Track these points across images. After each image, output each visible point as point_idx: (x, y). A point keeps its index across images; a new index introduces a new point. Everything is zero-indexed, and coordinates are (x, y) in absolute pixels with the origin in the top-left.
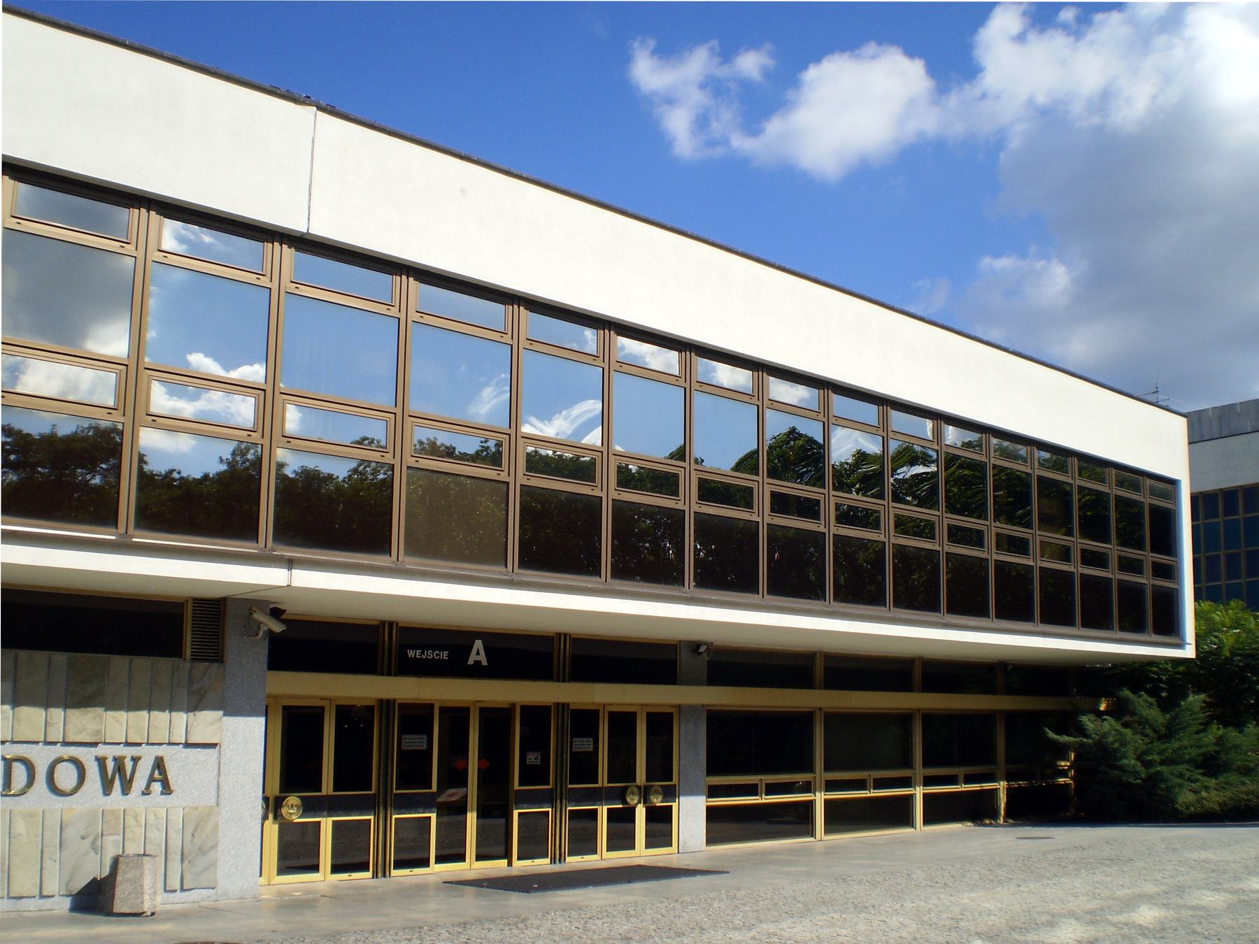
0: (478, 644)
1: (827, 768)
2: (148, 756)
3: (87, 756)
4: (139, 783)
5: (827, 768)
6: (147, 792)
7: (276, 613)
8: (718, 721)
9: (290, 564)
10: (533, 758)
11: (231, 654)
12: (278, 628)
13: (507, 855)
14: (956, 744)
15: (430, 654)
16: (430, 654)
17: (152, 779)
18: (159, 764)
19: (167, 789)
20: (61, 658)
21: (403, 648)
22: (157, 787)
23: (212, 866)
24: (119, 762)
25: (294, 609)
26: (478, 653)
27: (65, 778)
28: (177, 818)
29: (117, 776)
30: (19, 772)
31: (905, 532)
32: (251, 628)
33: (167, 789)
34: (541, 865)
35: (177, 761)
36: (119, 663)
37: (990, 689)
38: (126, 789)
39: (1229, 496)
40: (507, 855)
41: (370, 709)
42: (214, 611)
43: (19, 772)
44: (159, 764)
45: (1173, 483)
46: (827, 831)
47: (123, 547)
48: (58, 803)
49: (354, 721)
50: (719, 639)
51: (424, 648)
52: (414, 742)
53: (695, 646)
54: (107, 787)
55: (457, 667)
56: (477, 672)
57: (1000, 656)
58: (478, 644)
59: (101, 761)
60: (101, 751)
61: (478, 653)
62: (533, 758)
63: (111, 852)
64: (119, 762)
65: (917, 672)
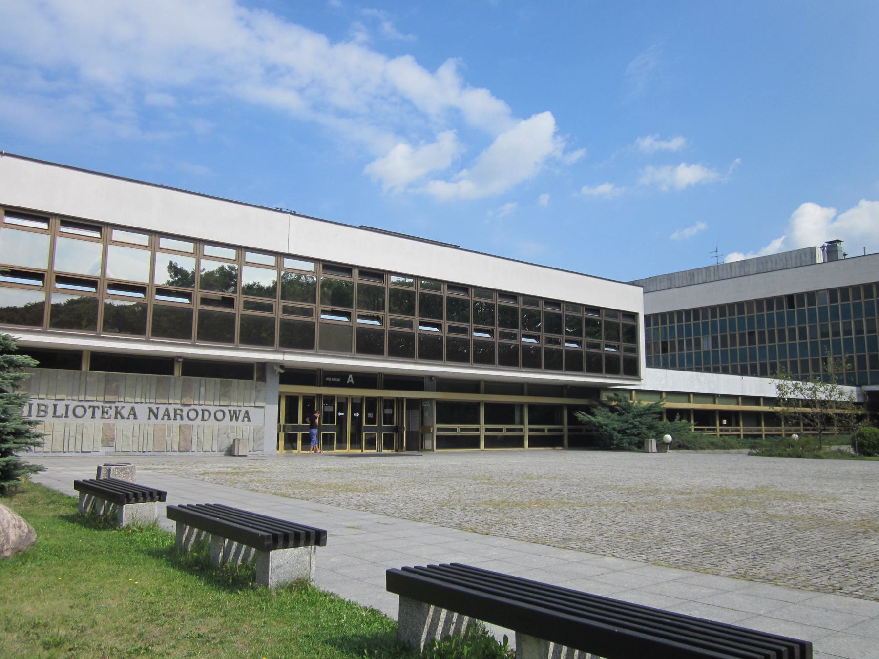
0: (350, 376)
1: (529, 423)
2: (244, 410)
3: (226, 409)
4: (241, 418)
5: (529, 423)
6: (163, 419)
7: (282, 367)
8: (440, 404)
9: (284, 353)
10: (370, 415)
11: (268, 380)
12: (282, 371)
13: (361, 448)
14: (500, 414)
15: (334, 379)
16: (334, 379)
17: (244, 417)
18: (247, 412)
19: (249, 420)
20: (218, 380)
21: (325, 379)
22: (246, 419)
23: (262, 444)
24: (235, 411)
25: (286, 365)
26: (350, 379)
27: (220, 415)
28: (252, 429)
29: (234, 416)
30: (206, 414)
31: (512, 334)
32: (274, 371)
33: (249, 420)
34: (359, 451)
35: (252, 412)
36: (235, 381)
37: (560, 395)
38: (237, 419)
39: (655, 316)
40: (361, 448)
41: (314, 397)
42: (263, 366)
43: (206, 414)
44: (247, 412)
45: (637, 314)
46: (486, 447)
47: (98, 337)
48: (217, 423)
49: (309, 401)
50: (440, 375)
51: (332, 377)
52: (388, 411)
53: (431, 378)
54: (231, 420)
55: (343, 384)
56: (350, 386)
57: (378, 371)
58: (350, 376)
59: (230, 411)
60: (230, 408)
61: (350, 379)
62: (370, 415)
63: (232, 437)
64: (235, 411)
65: (526, 388)
